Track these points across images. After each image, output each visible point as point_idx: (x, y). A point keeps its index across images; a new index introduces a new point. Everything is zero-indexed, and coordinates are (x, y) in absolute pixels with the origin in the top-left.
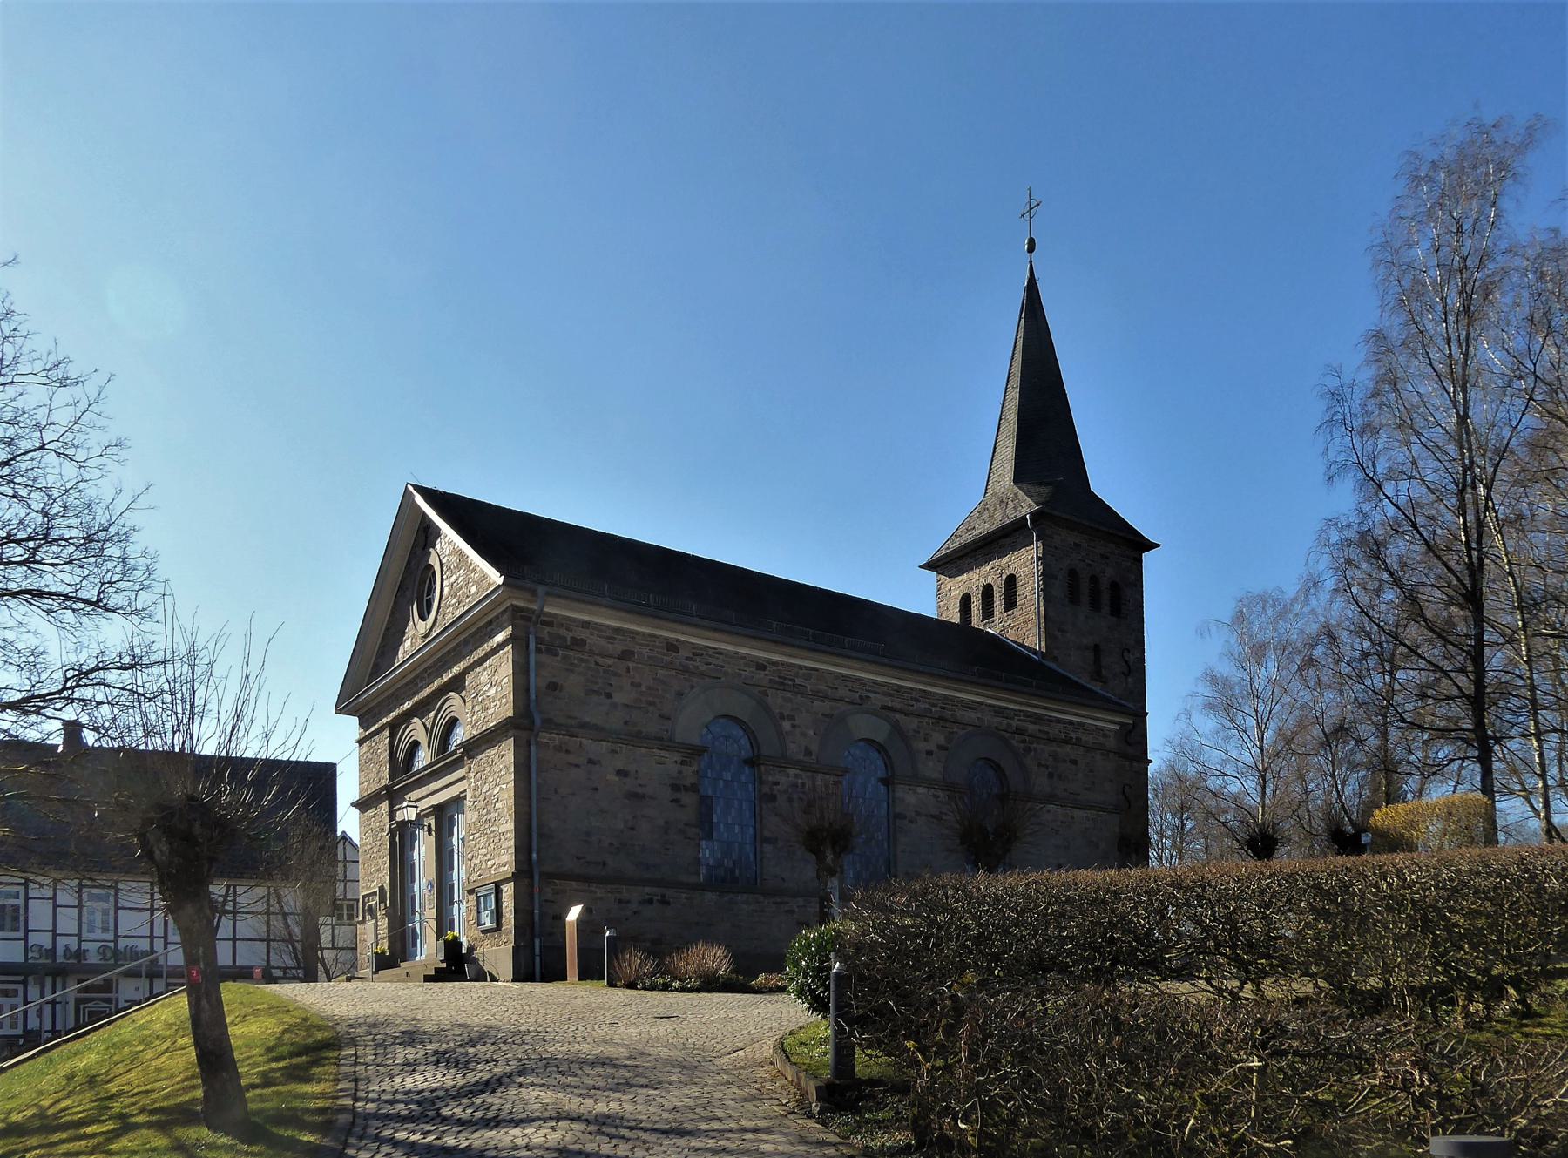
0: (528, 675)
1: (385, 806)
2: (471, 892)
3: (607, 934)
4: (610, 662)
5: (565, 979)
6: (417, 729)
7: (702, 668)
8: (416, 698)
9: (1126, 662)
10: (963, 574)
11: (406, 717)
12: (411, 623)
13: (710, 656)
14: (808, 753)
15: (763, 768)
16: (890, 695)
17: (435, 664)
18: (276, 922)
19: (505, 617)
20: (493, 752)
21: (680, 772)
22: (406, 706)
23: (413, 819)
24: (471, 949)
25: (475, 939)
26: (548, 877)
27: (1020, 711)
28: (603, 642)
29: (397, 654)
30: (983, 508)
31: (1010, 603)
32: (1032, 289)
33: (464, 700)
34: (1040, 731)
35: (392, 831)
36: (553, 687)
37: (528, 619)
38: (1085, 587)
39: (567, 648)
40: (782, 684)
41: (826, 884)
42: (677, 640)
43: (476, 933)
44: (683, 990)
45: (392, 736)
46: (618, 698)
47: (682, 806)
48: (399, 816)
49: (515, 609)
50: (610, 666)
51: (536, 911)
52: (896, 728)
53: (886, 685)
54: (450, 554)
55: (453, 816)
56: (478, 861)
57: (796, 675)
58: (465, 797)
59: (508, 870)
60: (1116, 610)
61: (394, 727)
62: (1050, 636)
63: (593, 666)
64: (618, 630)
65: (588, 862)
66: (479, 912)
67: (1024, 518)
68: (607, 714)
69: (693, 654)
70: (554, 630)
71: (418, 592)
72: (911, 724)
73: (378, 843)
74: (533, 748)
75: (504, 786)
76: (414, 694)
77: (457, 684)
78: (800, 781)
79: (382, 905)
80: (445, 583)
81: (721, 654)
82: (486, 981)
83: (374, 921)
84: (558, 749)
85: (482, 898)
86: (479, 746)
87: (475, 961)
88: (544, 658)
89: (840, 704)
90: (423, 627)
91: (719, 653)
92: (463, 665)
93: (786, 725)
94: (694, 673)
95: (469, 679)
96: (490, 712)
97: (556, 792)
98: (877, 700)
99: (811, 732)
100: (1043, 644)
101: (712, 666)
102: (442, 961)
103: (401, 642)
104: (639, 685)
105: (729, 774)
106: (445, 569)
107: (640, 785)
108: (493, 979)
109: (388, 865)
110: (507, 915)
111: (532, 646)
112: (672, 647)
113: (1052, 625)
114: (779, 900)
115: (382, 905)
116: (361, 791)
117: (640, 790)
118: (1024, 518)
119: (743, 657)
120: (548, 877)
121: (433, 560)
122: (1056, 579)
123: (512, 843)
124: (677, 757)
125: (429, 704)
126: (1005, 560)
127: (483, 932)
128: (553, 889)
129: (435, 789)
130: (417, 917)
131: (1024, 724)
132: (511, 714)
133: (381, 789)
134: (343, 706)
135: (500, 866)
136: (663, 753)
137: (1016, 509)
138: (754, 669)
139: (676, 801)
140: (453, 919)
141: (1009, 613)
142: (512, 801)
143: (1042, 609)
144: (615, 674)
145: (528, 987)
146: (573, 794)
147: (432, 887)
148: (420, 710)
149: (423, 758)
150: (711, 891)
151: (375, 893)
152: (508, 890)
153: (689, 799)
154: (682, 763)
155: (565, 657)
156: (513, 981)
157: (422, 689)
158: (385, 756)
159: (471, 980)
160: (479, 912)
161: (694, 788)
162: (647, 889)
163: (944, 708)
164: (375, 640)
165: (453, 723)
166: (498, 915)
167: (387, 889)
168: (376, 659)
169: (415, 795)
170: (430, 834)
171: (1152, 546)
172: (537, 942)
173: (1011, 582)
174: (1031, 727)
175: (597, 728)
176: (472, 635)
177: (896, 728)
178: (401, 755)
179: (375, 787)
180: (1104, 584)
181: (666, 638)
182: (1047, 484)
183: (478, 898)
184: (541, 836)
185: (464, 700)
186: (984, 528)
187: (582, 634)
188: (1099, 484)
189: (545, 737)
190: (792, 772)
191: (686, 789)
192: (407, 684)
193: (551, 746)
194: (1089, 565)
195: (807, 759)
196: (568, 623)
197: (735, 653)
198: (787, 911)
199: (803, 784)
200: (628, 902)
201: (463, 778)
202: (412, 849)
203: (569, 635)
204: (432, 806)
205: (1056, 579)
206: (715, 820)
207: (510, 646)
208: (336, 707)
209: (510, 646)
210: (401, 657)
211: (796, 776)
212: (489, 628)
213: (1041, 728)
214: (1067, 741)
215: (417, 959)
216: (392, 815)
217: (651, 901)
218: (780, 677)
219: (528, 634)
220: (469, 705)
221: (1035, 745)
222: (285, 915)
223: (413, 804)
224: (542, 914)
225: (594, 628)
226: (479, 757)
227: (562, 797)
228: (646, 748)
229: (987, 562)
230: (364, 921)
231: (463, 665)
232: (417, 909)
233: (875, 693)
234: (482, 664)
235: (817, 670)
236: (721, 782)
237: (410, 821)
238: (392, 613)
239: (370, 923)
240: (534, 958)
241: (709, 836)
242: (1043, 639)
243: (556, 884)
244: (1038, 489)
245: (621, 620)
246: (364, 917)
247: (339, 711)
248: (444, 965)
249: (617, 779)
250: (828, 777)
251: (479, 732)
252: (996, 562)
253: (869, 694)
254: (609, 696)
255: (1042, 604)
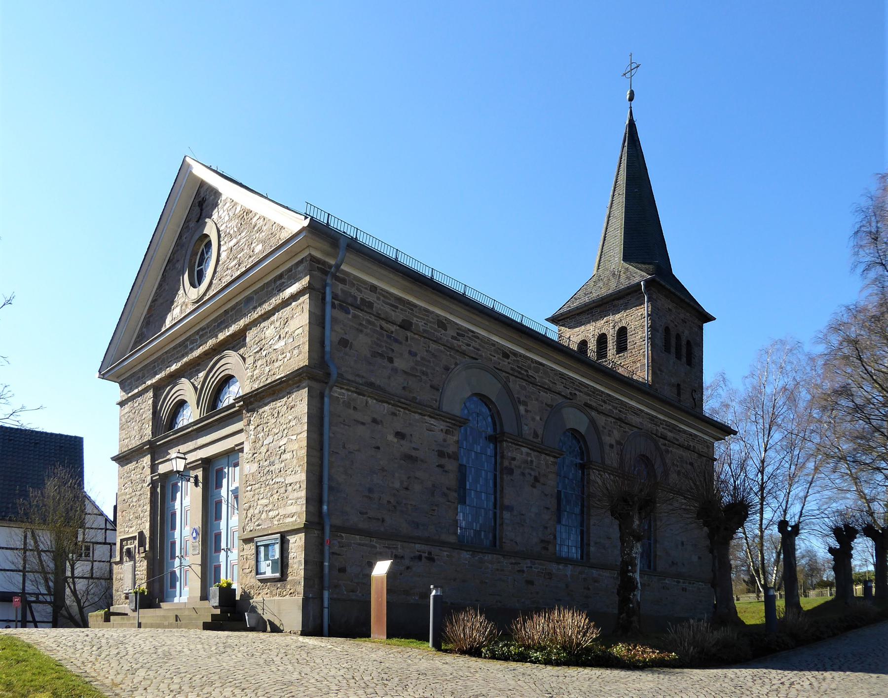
0: (324, 328)
1: (147, 460)
2: (247, 541)
3: (434, 593)
4: (393, 328)
5: (369, 636)
6: (185, 389)
7: (464, 347)
8: (185, 360)
9: (694, 399)
10: (580, 326)
11: (173, 379)
12: (181, 292)
13: (469, 338)
14: (536, 435)
15: (505, 444)
16: (589, 395)
17: (208, 326)
18: (32, 558)
19: (300, 268)
20: (279, 404)
21: (445, 440)
22: (174, 367)
23: (182, 470)
24: (246, 596)
25: (252, 587)
26: (337, 529)
27: (664, 421)
28: (387, 308)
29: (165, 322)
30: (599, 279)
31: (622, 347)
32: (632, 125)
33: (244, 359)
34: (674, 438)
35: (153, 484)
36: (344, 343)
37: (325, 273)
38: (673, 341)
39: (358, 308)
40: (520, 373)
41: (631, 550)
42: (446, 319)
43: (252, 580)
44: (548, 662)
45: (156, 397)
46: (399, 363)
47: (446, 471)
48: (163, 469)
49: (313, 259)
50: (392, 332)
51: (326, 564)
52: (593, 422)
53: (587, 386)
54: (230, 220)
55: (176, 484)
56: (257, 511)
57: (530, 367)
58: (242, 450)
59: (300, 520)
60: (689, 362)
61: (158, 389)
62: (654, 373)
63: (378, 329)
64: (400, 300)
65: (369, 518)
66: (257, 561)
67: (639, 284)
68: (389, 378)
69: (458, 334)
70: (346, 288)
71: (190, 260)
72: (601, 420)
73: (138, 493)
74: (326, 400)
75: (294, 437)
76: (183, 356)
77: (237, 341)
78: (529, 459)
79: (142, 549)
80: (223, 248)
81: (478, 338)
82: (265, 631)
83: (132, 563)
84: (347, 405)
85: (262, 549)
86: (262, 398)
87: (253, 610)
88: (338, 314)
89: (557, 397)
90: (194, 293)
91: (476, 336)
92: (242, 323)
93: (522, 409)
94: (458, 351)
95: (250, 336)
96: (276, 364)
97: (344, 447)
98: (582, 398)
99: (538, 418)
100: (650, 379)
101: (471, 348)
102: (215, 607)
103: (169, 309)
104: (415, 355)
105: (479, 448)
106: (222, 235)
107: (414, 449)
108: (275, 629)
109: (148, 513)
110: (295, 566)
111: (328, 298)
112: (442, 324)
113: (656, 366)
114: (514, 561)
115: (142, 549)
116: (121, 447)
117: (414, 453)
118: (639, 284)
119: (494, 344)
120: (337, 529)
121: (210, 229)
122: (658, 332)
123: (303, 493)
124: (442, 426)
125: (199, 364)
126: (617, 316)
127: (261, 581)
128: (339, 542)
129: (204, 442)
130: (177, 562)
131: (665, 431)
132: (307, 363)
133: (144, 444)
134: (105, 373)
135: (285, 516)
136: (432, 421)
137: (628, 278)
138: (501, 357)
139: (440, 466)
140: (220, 566)
141: (620, 355)
142: (304, 452)
143: (650, 352)
144: (396, 341)
145: (311, 641)
146: (359, 450)
147: (197, 534)
148: (189, 371)
149: (189, 415)
150: (467, 551)
151: (134, 538)
152: (297, 543)
153: (451, 466)
154: (447, 432)
155: (355, 316)
156: (304, 633)
157: (192, 350)
158: (149, 415)
159: (252, 629)
160: (257, 561)
161: (454, 457)
162: (418, 546)
163: (620, 411)
164: (142, 311)
165: (228, 380)
166: (283, 565)
167: (147, 534)
168: (141, 328)
169: (184, 448)
170: (196, 484)
171: (709, 318)
172: (326, 594)
173: (622, 333)
174: (669, 434)
175: (379, 388)
176: (256, 292)
177: (593, 422)
178: (164, 414)
179: (135, 443)
180: (684, 343)
181: (438, 316)
182: (649, 264)
183: (257, 547)
184: (331, 488)
185: (244, 359)
186: (602, 291)
187: (371, 297)
188: (678, 271)
189: (337, 392)
190: (524, 450)
191: (449, 457)
192: (174, 348)
193: (341, 400)
194: (676, 326)
195: (535, 440)
196: (360, 284)
197: (489, 339)
198: (519, 571)
199: (532, 461)
200: (402, 557)
201: (240, 431)
202: (174, 499)
203: (359, 296)
204: (201, 459)
205: (658, 332)
206: (468, 487)
207: (307, 296)
208: (100, 372)
209: (307, 296)
210: (168, 323)
211: (528, 454)
212: (278, 283)
213: (675, 436)
214: (688, 448)
215: (176, 600)
216: (154, 468)
217: (420, 558)
218: (518, 367)
219: (324, 287)
220: (250, 361)
221: (671, 449)
222: (39, 552)
223: (182, 456)
224: (331, 567)
225: (380, 294)
226: (261, 411)
227: (350, 452)
228: (420, 414)
229: (602, 317)
230: (121, 562)
231: (242, 323)
232: (178, 553)
233: (580, 391)
234: (268, 318)
235: (543, 365)
236: (473, 453)
237: (178, 472)
238: (160, 285)
239: (128, 565)
240: (322, 611)
241: (462, 500)
242: (650, 375)
243: (342, 536)
244: (647, 266)
245: (404, 290)
246: (121, 558)
247: (103, 375)
248: (218, 611)
249: (395, 440)
250: (548, 458)
251: (262, 385)
252: (611, 318)
253: (577, 393)
254: (391, 360)
255: (650, 349)
